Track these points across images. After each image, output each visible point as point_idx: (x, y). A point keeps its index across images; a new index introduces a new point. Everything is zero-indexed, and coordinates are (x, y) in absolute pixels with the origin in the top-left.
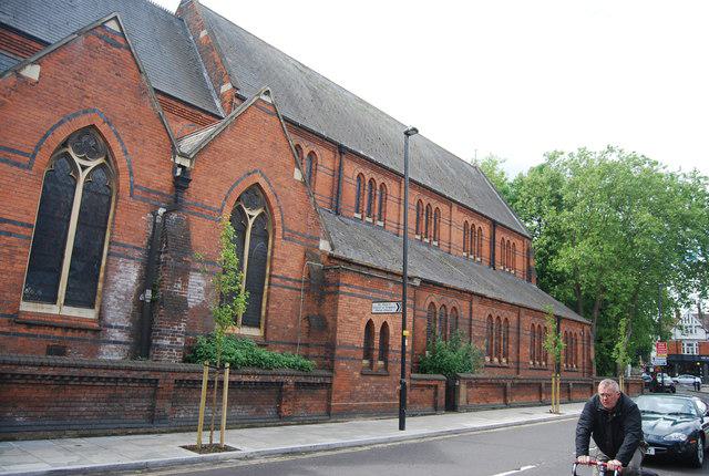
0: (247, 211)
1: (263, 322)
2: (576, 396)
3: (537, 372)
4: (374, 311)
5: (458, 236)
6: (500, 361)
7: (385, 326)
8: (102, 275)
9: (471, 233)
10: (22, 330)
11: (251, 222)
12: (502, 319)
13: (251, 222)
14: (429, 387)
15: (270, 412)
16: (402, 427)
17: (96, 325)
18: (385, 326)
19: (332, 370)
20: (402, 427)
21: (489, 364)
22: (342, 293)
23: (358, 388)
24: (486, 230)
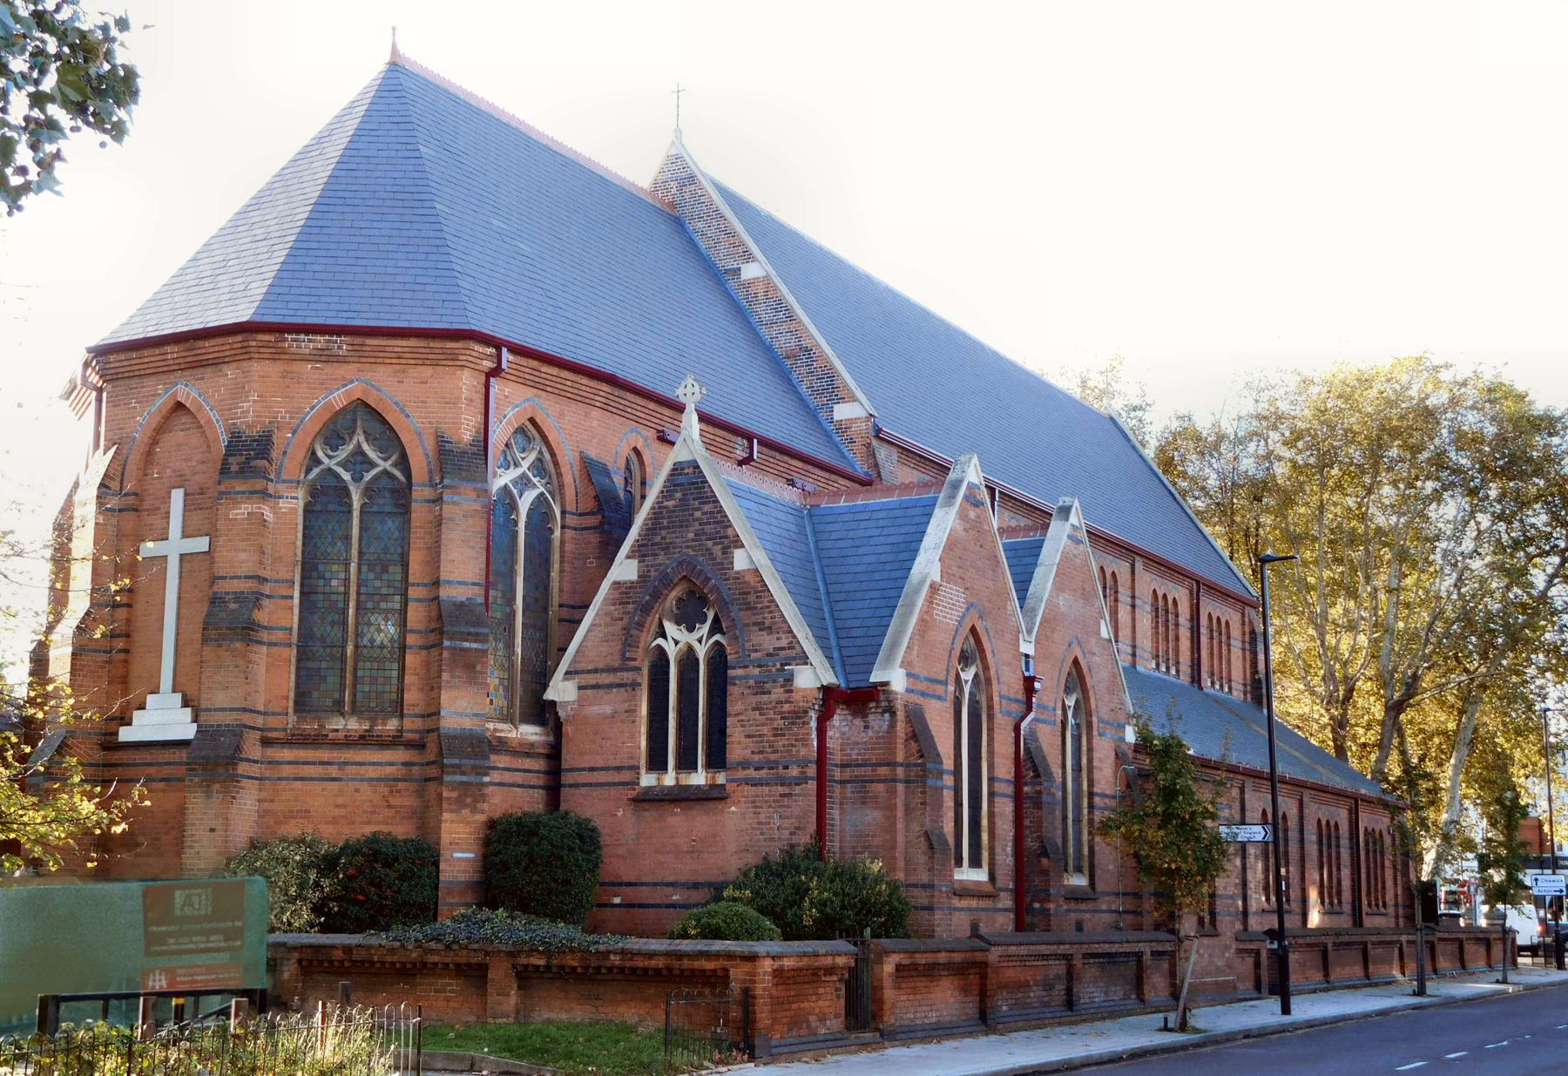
1: (985, 855)
9: (1163, 610)
11: (967, 689)
13: (967, 689)
16: (1286, 1010)
17: (989, 888)
20: (1286, 1010)
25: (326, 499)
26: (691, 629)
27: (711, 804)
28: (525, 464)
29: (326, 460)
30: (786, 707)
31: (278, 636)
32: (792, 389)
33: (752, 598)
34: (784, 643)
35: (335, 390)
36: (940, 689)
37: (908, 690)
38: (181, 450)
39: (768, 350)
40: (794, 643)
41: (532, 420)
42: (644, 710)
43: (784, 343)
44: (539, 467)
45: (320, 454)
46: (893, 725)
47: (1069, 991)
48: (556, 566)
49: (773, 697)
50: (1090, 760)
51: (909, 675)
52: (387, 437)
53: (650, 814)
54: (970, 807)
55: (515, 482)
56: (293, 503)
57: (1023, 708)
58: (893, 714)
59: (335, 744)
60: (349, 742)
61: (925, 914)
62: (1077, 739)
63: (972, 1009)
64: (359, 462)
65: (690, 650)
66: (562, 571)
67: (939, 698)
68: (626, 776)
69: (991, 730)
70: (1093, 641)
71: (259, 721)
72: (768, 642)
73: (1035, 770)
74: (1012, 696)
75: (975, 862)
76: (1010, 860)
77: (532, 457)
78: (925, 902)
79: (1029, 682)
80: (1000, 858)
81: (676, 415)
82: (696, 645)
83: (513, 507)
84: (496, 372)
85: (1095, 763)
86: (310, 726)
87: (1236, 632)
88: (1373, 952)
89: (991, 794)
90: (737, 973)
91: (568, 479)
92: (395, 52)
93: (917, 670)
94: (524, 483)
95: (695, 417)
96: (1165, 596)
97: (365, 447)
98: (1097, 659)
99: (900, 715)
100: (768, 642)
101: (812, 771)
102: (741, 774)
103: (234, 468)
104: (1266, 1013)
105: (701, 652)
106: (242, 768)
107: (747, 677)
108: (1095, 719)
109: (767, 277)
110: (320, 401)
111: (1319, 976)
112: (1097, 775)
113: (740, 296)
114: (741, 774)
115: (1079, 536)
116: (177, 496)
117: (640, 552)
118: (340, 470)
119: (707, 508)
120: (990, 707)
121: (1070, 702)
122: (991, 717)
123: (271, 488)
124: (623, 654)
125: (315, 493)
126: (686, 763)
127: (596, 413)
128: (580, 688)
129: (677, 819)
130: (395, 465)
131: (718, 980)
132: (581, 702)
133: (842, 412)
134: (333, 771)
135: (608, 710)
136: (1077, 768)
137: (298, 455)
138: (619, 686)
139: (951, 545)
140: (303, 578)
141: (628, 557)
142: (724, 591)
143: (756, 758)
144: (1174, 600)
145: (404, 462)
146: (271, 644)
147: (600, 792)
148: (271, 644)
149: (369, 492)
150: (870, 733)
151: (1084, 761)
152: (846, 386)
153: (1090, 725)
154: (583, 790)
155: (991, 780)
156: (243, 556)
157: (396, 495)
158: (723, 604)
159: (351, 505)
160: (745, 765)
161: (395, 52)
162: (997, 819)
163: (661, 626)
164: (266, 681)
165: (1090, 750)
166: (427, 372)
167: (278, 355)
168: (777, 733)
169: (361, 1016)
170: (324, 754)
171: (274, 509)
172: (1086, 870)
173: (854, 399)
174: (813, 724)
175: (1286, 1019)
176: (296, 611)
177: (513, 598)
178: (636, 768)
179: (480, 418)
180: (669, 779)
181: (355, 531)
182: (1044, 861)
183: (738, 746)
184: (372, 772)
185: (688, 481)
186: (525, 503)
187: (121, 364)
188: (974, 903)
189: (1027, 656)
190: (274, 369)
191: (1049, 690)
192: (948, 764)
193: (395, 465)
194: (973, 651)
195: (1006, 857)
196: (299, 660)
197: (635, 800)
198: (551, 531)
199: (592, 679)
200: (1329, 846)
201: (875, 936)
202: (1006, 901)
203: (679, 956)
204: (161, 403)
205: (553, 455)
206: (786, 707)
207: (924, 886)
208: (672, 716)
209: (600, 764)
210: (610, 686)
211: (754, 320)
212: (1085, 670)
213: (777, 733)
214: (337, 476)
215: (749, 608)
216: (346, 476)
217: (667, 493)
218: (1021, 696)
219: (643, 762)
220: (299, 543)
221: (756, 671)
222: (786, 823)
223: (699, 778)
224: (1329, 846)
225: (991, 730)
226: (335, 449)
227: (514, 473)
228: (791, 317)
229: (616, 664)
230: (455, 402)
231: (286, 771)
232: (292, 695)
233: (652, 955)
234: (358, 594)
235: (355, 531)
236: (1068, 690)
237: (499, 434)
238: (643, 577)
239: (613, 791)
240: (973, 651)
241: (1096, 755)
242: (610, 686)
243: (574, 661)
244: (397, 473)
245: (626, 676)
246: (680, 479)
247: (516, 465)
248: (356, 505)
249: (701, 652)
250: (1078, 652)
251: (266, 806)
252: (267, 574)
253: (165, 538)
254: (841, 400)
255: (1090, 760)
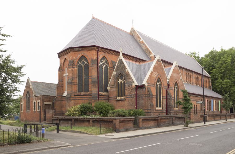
0: (158, 84)
1: (162, 106)
2: (216, 119)
3: (217, 113)
4: (197, 103)
5: (195, 80)
6: (210, 111)
7: (196, 105)
8: (161, 102)
9: (197, 79)
10: (156, 112)
11: (158, 86)
12: (210, 101)
13: (158, 86)
14: (224, 115)
15: (219, 118)
16: (205, 124)
17: (162, 110)
18: (196, 105)
19: (190, 114)
20: (205, 124)
21: (201, 111)
22: (155, 96)
23: (194, 117)
24: (200, 77)
25: (80, 67)
26: (122, 80)
27: (124, 101)
28: (104, 62)
29: (80, 63)
30: (132, 88)
31: (76, 83)
32: (145, 53)
33: (128, 75)
34: (131, 80)
35: (80, 55)
36: (153, 85)
37: (148, 85)
38: (67, 64)
39: (142, 49)
40: (132, 80)
41: (104, 56)
42: (117, 90)
43: (145, 48)
44: (106, 62)
45: (79, 62)
46: (145, 90)
47: (173, 122)
48: (109, 74)
49: (130, 87)
50: (179, 94)
51: (148, 83)
52: (86, 60)
53: (118, 102)
54: (159, 100)
55: (102, 64)
56: (76, 68)
57: (167, 88)
58: (145, 88)
59: (82, 95)
60: (83, 95)
61: (150, 113)
62: (177, 92)
63: (156, 125)
64: (83, 63)
65: (122, 82)
66: (109, 74)
67: (153, 86)
68: (115, 98)
69: (162, 90)
70: (179, 79)
71: (74, 93)
72: (130, 80)
73: (169, 95)
74: (166, 86)
75: (160, 107)
76: (165, 106)
77: (105, 61)
78: (150, 112)
79: (168, 85)
80: (164, 106)
81: (119, 54)
82: (122, 82)
83: (102, 67)
84: (98, 51)
85: (179, 95)
86: (79, 94)
87: (207, 81)
88: (221, 116)
89: (162, 98)
90: (114, 121)
91: (110, 63)
92: (93, 17)
93: (149, 83)
94: (104, 64)
95: (122, 53)
96: (197, 77)
97: (84, 61)
98: (180, 82)
99: (146, 88)
100: (130, 80)
101: (135, 96)
102: (127, 97)
103: (69, 65)
104: (202, 124)
105: (123, 82)
106: (71, 98)
107: (127, 85)
108: (179, 89)
109: (142, 41)
110: (78, 56)
111: (213, 119)
112: (180, 96)
113: (140, 44)
114: (127, 97)
115: (177, 66)
116: (66, 69)
117: (116, 71)
118: (81, 64)
119: (123, 64)
120: (162, 88)
121: (176, 87)
122: (162, 89)
123: (74, 67)
124: (115, 83)
125: (79, 66)
126: (122, 96)
127: (113, 55)
128: (110, 88)
129: (120, 102)
130: (87, 63)
131: (112, 122)
132: (111, 89)
133: (151, 56)
134: (82, 98)
135: (113, 90)
136: (177, 95)
137: (76, 62)
138: (114, 87)
139: (155, 67)
140: (78, 77)
141: (115, 72)
142: (125, 75)
143: (129, 95)
144: (190, 74)
145: (88, 62)
146: (74, 84)
147: (112, 100)
148: (74, 84)
149: (84, 66)
150: (143, 91)
151: (178, 94)
152: (151, 52)
153: (179, 90)
154: (111, 100)
155: (162, 97)
156: (71, 75)
157: (87, 66)
158: (125, 76)
159: (82, 68)
160: (127, 96)
161: (93, 17)
162: (163, 101)
163: (118, 80)
164: (75, 88)
165: (179, 93)
166: (90, 51)
167: (74, 51)
168: (131, 91)
169: (154, 121)
170: (81, 97)
171: (74, 69)
172: (178, 107)
173: (152, 54)
174: (135, 90)
175: (205, 125)
176: (77, 80)
177: (103, 78)
178: (116, 97)
179: (97, 56)
180: (120, 98)
181: (83, 71)
182: (170, 106)
183: (127, 94)
184: (86, 98)
185: (121, 61)
186: (104, 67)
187: (61, 55)
188: (159, 112)
189: (168, 81)
190: (73, 53)
191: (172, 85)
192: (173, 96)
193: (87, 63)
194: (159, 80)
195: (165, 106)
196: (78, 86)
197: (116, 101)
198: (108, 70)
199: (111, 87)
200: (217, 104)
201: (139, 116)
202: (165, 111)
203: (108, 119)
204: (64, 59)
205: (108, 61)
206: (132, 88)
207: (150, 110)
208: (120, 90)
209: (113, 97)
210: (113, 87)
211: (141, 46)
212: (178, 83)
213: (131, 91)
214: (81, 65)
215: (127, 76)
216: (82, 65)
217: (118, 63)
218: (167, 86)
219: (117, 96)
220: (77, 73)
221: (128, 84)
222: (132, 103)
223: (123, 98)
224: (217, 104)
225: (162, 90)
226: (81, 61)
227: (102, 63)
228: (145, 45)
229: (114, 85)
230: (93, 55)
231: (77, 99)
232: (77, 90)
233: (105, 119)
234: (84, 78)
235: (83, 71)
236: (175, 85)
237: (100, 58)
238: (116, 74)
239: (114, 100)
240: (159, 80)
241: (179, 94)
242: (113, 87)
243: (109, 85)
244: (88, 64)
245: (115, 86)
246: (120, 61)
247: (103, 62)
248: (83, 68)
249: (123, 82)
250: (177, 81)
251: (75, 103)
252: (74, 76)
253: (65, 74)
254: (151, 54)
255: (179, 94)
